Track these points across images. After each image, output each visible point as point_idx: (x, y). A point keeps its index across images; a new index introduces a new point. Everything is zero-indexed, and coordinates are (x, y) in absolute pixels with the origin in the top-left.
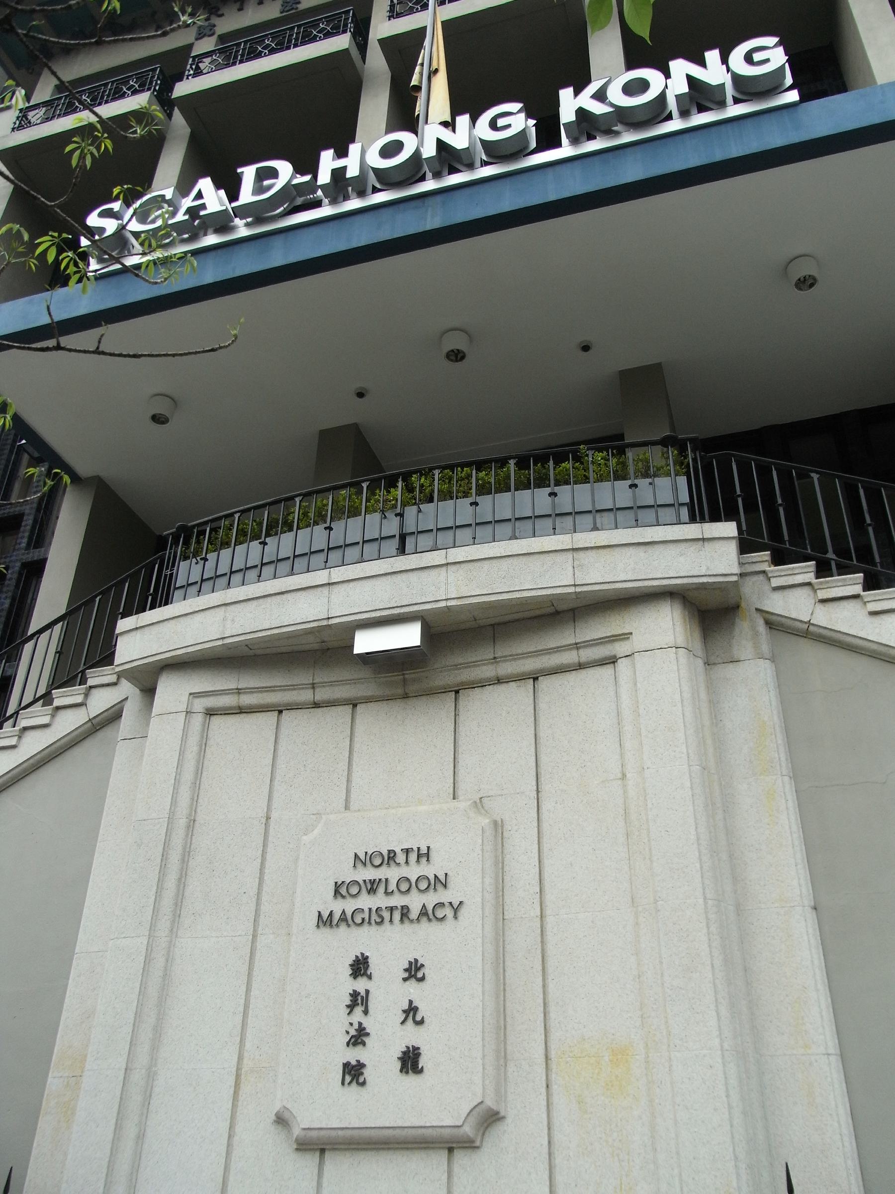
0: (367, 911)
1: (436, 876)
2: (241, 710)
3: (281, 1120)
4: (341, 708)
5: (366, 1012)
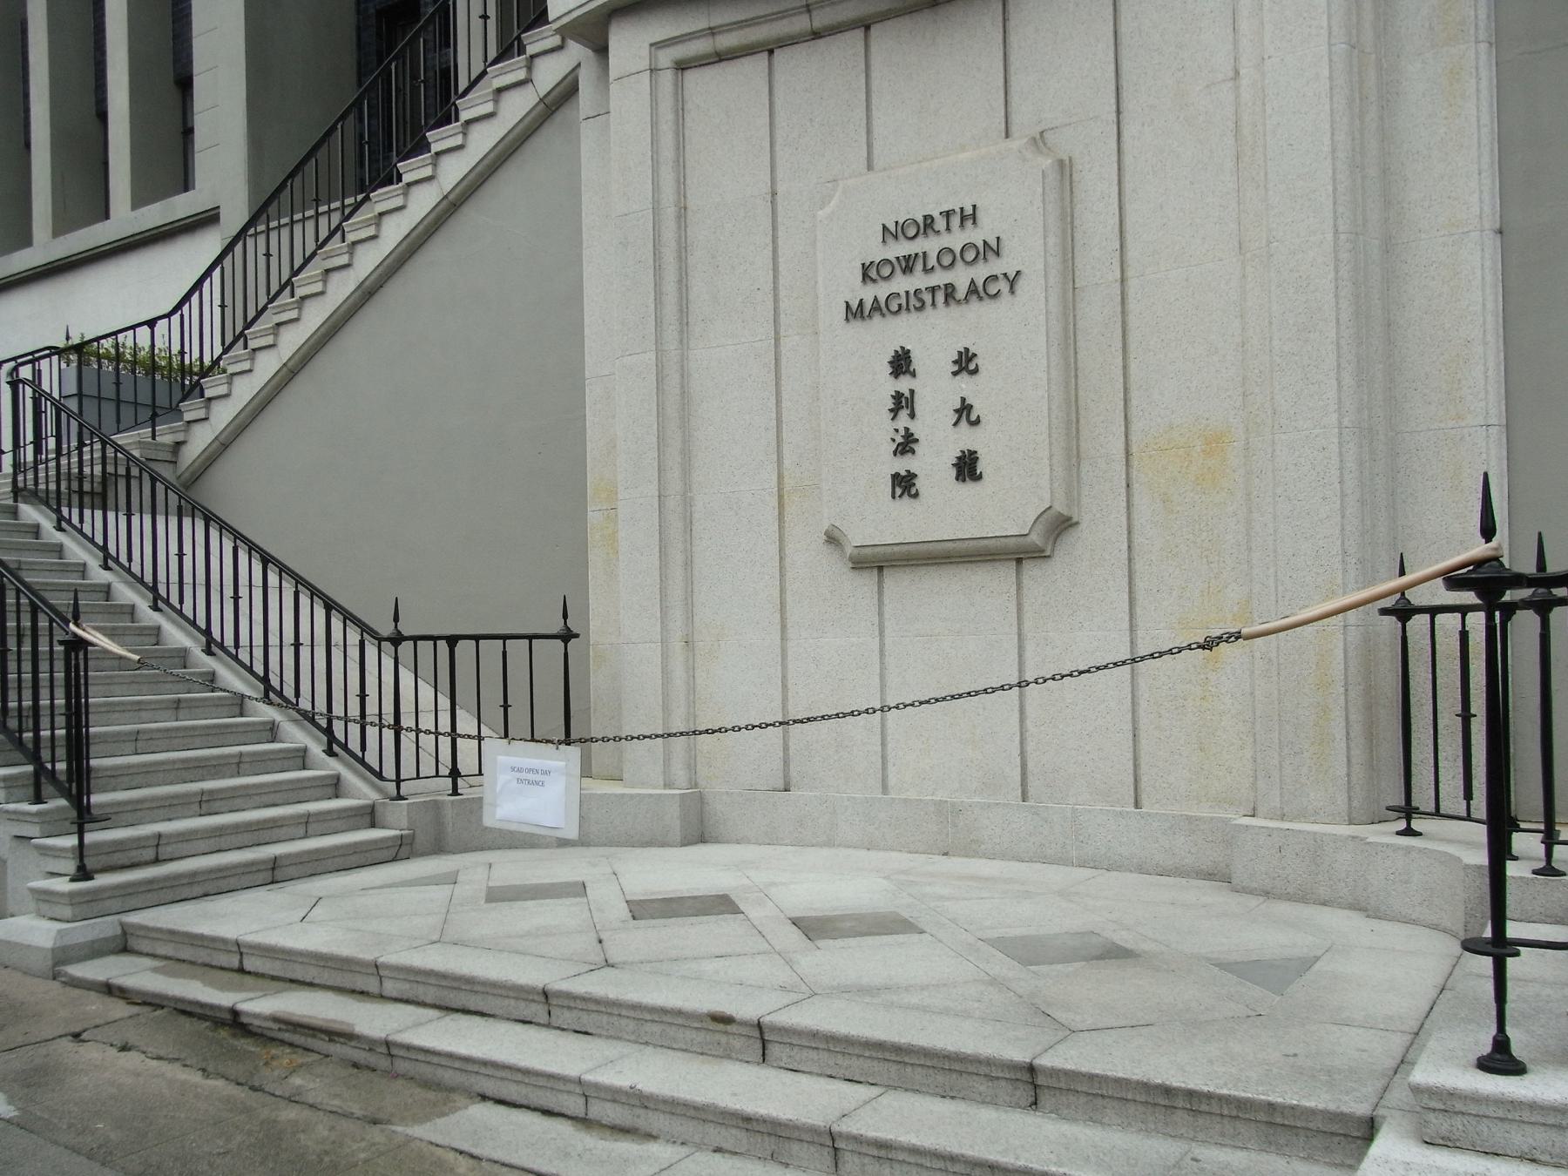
0: (903, 295)
2: (720, 57)
3: (833, 539)
4: (848, 35)
5: (912, 416)
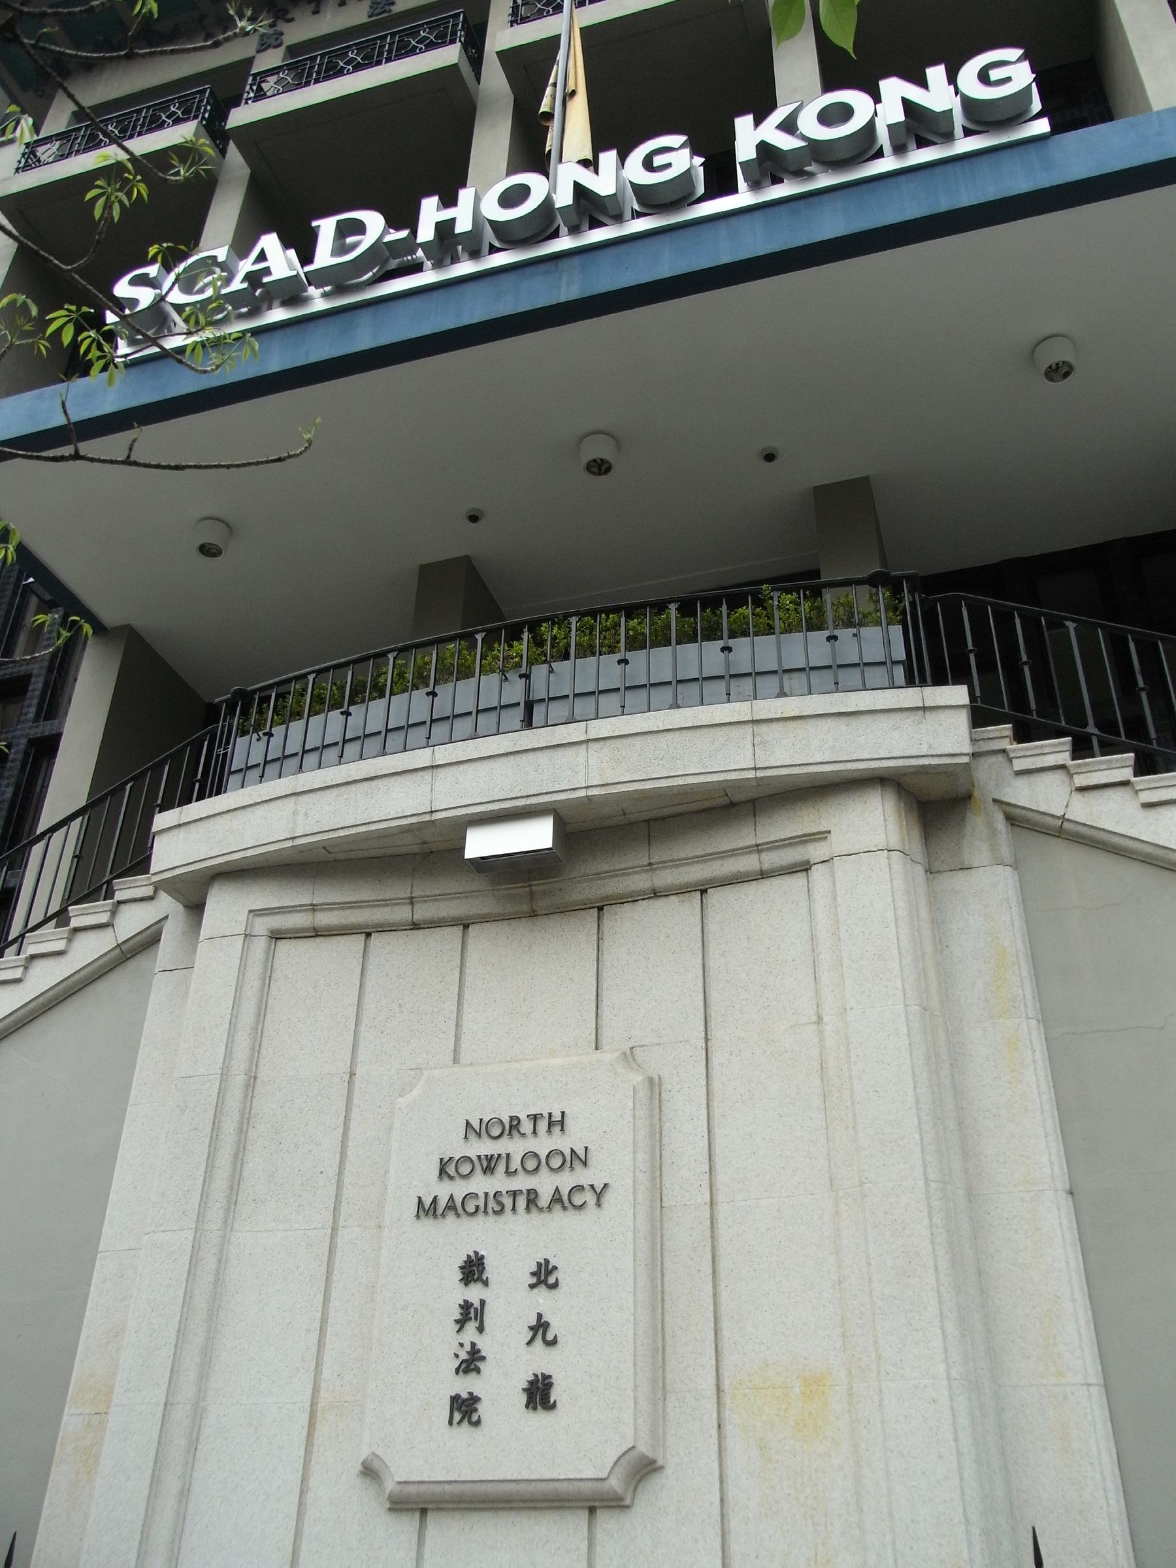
0: (482, 1196)
1: (572, 1151)
2: (317, 933)
3: (370, 1471)
4: (447, 930)
5: (481, 1329)
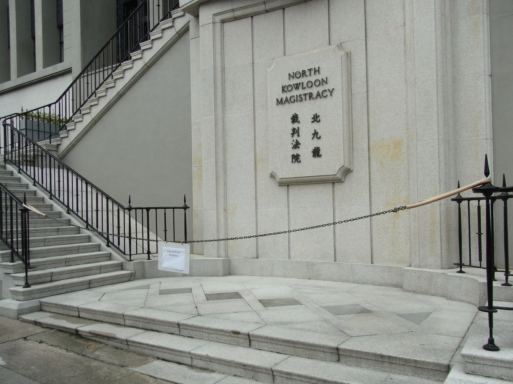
0: (295, 96)
2: (236, 19)
3: (272, 176)
4: (277, 11)
5: (298, 136)
